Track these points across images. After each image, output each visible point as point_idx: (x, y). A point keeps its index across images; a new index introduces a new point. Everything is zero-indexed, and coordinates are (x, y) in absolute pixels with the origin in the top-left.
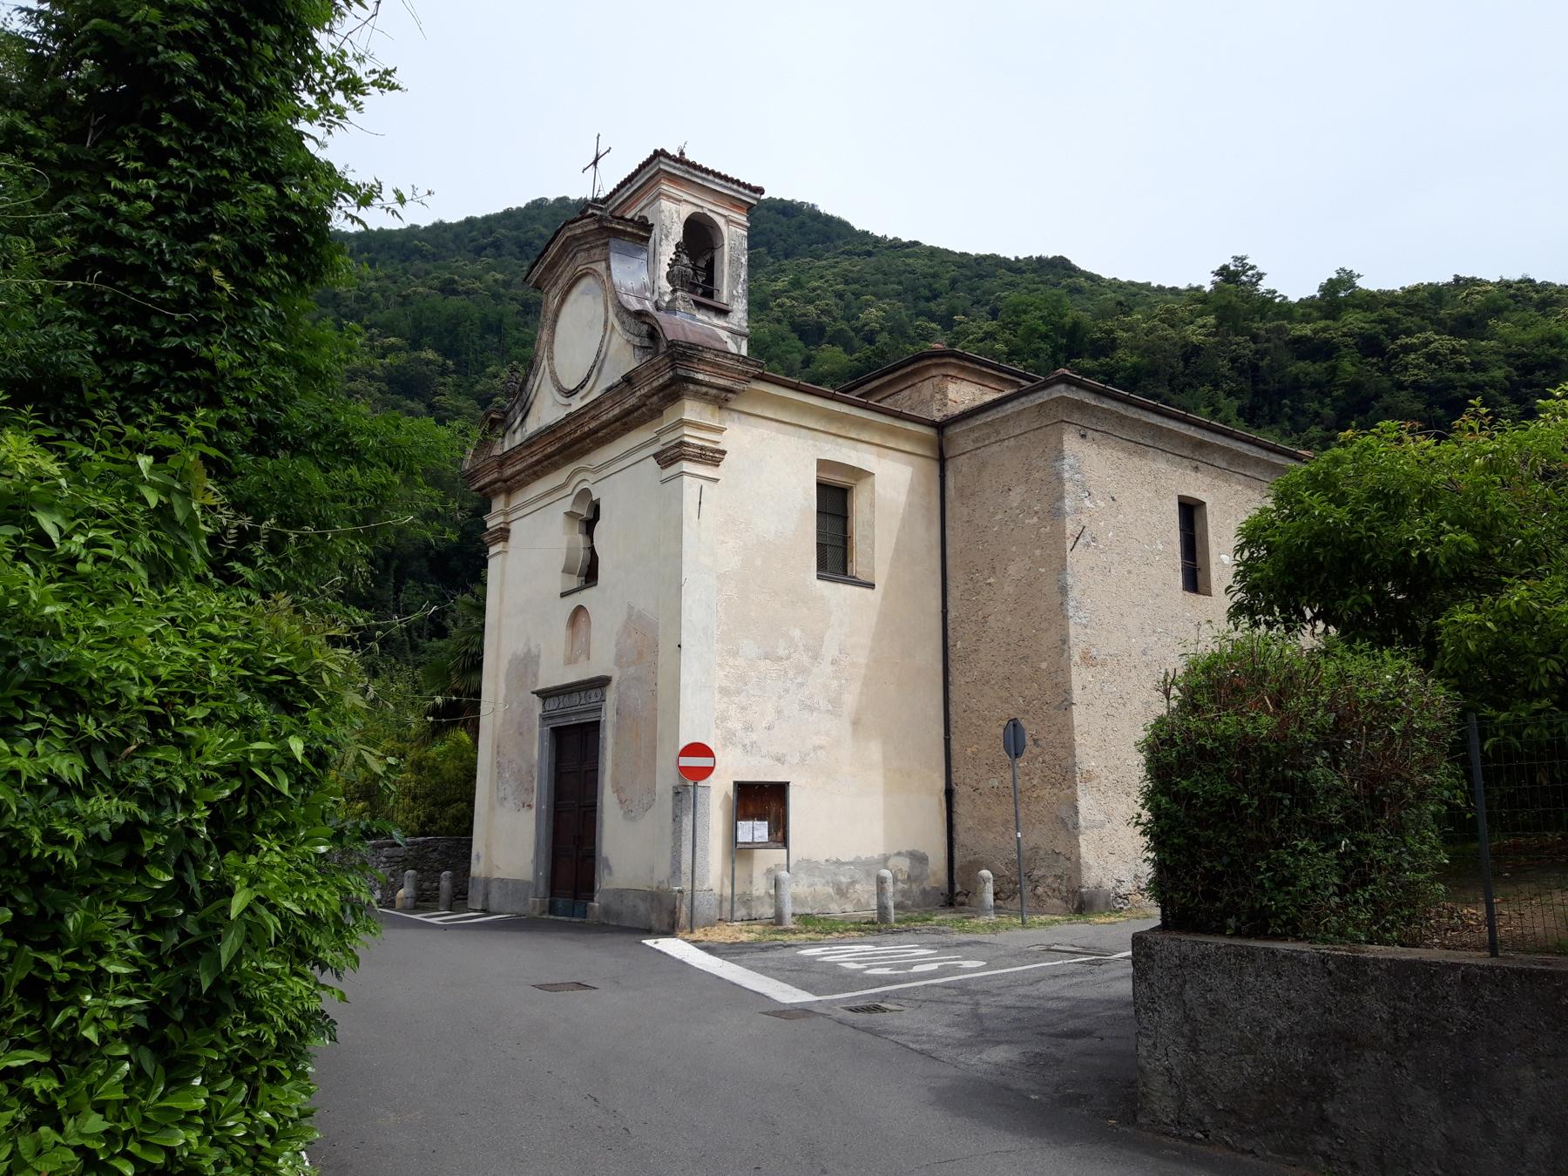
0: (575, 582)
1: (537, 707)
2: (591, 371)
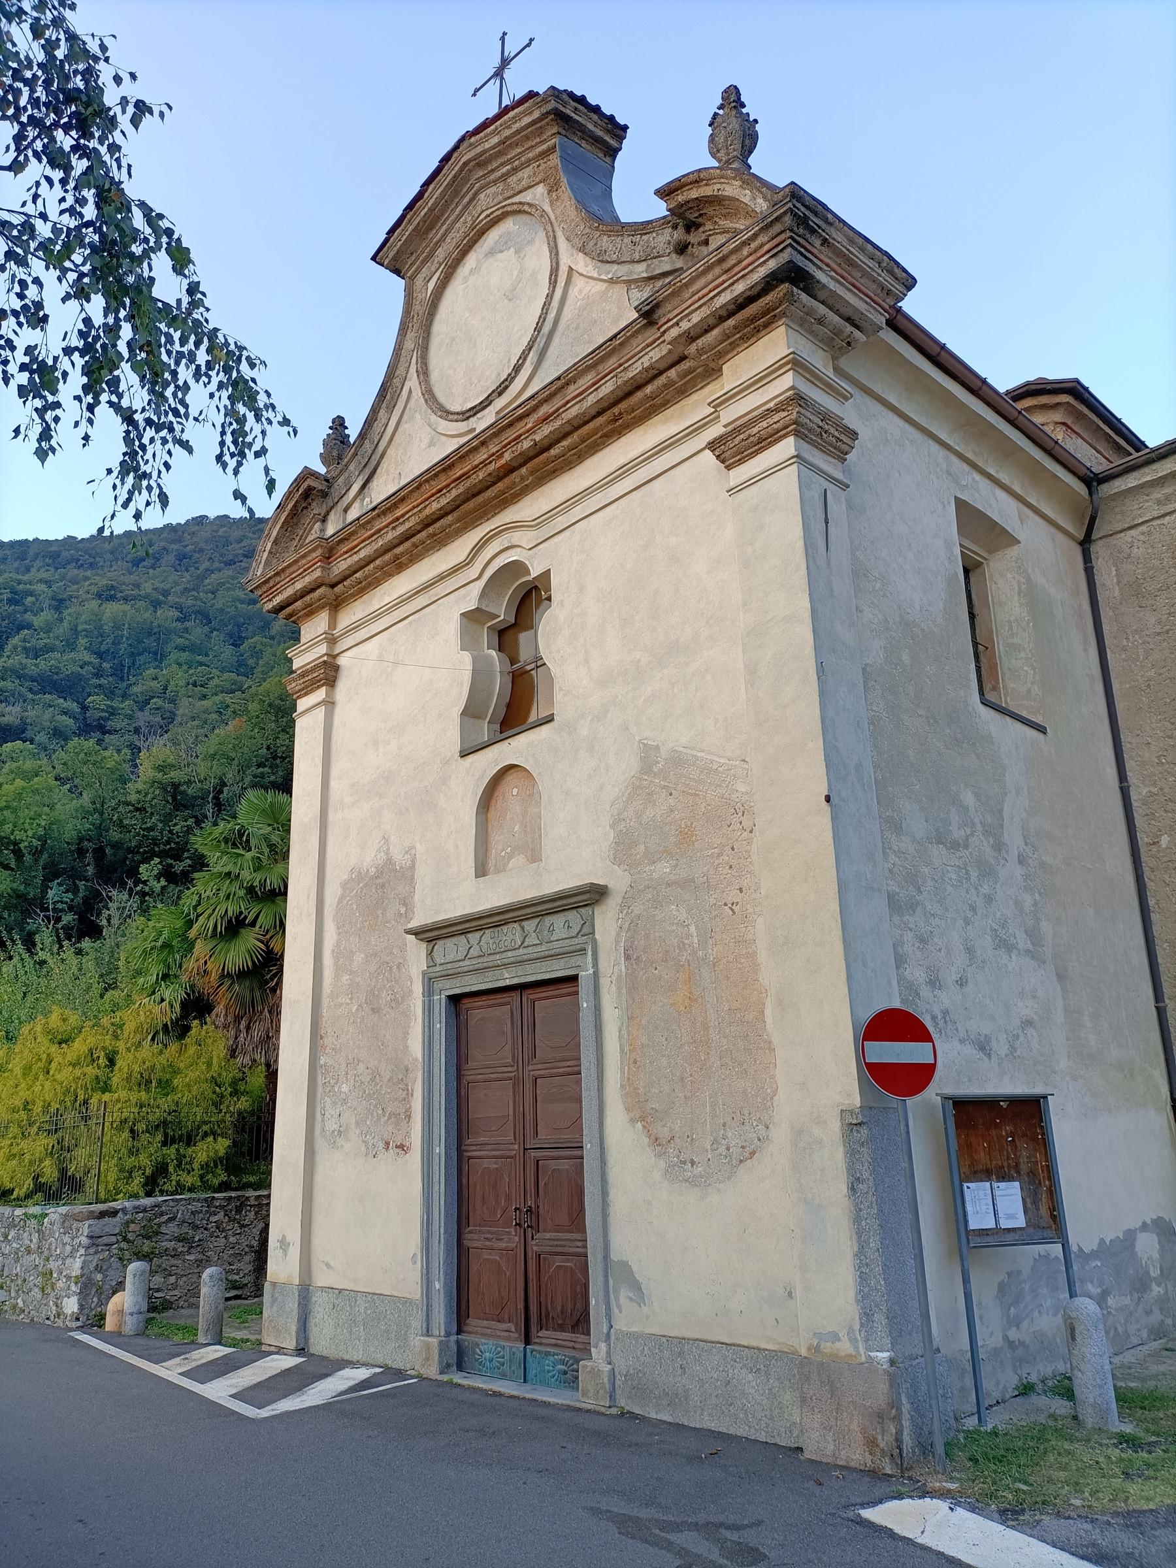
0: (485, 731)
1: (416, 955)
2: (524, 357)
